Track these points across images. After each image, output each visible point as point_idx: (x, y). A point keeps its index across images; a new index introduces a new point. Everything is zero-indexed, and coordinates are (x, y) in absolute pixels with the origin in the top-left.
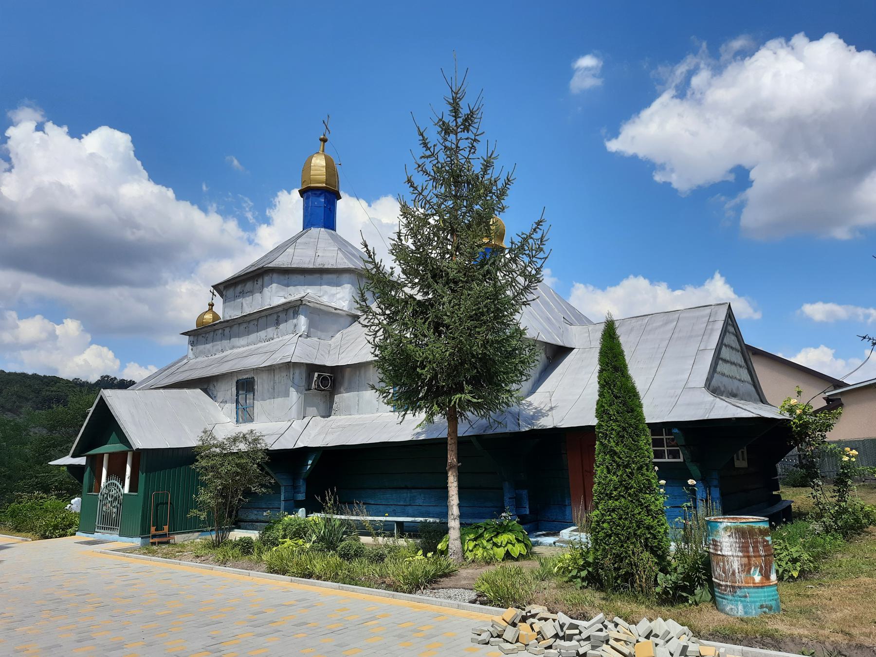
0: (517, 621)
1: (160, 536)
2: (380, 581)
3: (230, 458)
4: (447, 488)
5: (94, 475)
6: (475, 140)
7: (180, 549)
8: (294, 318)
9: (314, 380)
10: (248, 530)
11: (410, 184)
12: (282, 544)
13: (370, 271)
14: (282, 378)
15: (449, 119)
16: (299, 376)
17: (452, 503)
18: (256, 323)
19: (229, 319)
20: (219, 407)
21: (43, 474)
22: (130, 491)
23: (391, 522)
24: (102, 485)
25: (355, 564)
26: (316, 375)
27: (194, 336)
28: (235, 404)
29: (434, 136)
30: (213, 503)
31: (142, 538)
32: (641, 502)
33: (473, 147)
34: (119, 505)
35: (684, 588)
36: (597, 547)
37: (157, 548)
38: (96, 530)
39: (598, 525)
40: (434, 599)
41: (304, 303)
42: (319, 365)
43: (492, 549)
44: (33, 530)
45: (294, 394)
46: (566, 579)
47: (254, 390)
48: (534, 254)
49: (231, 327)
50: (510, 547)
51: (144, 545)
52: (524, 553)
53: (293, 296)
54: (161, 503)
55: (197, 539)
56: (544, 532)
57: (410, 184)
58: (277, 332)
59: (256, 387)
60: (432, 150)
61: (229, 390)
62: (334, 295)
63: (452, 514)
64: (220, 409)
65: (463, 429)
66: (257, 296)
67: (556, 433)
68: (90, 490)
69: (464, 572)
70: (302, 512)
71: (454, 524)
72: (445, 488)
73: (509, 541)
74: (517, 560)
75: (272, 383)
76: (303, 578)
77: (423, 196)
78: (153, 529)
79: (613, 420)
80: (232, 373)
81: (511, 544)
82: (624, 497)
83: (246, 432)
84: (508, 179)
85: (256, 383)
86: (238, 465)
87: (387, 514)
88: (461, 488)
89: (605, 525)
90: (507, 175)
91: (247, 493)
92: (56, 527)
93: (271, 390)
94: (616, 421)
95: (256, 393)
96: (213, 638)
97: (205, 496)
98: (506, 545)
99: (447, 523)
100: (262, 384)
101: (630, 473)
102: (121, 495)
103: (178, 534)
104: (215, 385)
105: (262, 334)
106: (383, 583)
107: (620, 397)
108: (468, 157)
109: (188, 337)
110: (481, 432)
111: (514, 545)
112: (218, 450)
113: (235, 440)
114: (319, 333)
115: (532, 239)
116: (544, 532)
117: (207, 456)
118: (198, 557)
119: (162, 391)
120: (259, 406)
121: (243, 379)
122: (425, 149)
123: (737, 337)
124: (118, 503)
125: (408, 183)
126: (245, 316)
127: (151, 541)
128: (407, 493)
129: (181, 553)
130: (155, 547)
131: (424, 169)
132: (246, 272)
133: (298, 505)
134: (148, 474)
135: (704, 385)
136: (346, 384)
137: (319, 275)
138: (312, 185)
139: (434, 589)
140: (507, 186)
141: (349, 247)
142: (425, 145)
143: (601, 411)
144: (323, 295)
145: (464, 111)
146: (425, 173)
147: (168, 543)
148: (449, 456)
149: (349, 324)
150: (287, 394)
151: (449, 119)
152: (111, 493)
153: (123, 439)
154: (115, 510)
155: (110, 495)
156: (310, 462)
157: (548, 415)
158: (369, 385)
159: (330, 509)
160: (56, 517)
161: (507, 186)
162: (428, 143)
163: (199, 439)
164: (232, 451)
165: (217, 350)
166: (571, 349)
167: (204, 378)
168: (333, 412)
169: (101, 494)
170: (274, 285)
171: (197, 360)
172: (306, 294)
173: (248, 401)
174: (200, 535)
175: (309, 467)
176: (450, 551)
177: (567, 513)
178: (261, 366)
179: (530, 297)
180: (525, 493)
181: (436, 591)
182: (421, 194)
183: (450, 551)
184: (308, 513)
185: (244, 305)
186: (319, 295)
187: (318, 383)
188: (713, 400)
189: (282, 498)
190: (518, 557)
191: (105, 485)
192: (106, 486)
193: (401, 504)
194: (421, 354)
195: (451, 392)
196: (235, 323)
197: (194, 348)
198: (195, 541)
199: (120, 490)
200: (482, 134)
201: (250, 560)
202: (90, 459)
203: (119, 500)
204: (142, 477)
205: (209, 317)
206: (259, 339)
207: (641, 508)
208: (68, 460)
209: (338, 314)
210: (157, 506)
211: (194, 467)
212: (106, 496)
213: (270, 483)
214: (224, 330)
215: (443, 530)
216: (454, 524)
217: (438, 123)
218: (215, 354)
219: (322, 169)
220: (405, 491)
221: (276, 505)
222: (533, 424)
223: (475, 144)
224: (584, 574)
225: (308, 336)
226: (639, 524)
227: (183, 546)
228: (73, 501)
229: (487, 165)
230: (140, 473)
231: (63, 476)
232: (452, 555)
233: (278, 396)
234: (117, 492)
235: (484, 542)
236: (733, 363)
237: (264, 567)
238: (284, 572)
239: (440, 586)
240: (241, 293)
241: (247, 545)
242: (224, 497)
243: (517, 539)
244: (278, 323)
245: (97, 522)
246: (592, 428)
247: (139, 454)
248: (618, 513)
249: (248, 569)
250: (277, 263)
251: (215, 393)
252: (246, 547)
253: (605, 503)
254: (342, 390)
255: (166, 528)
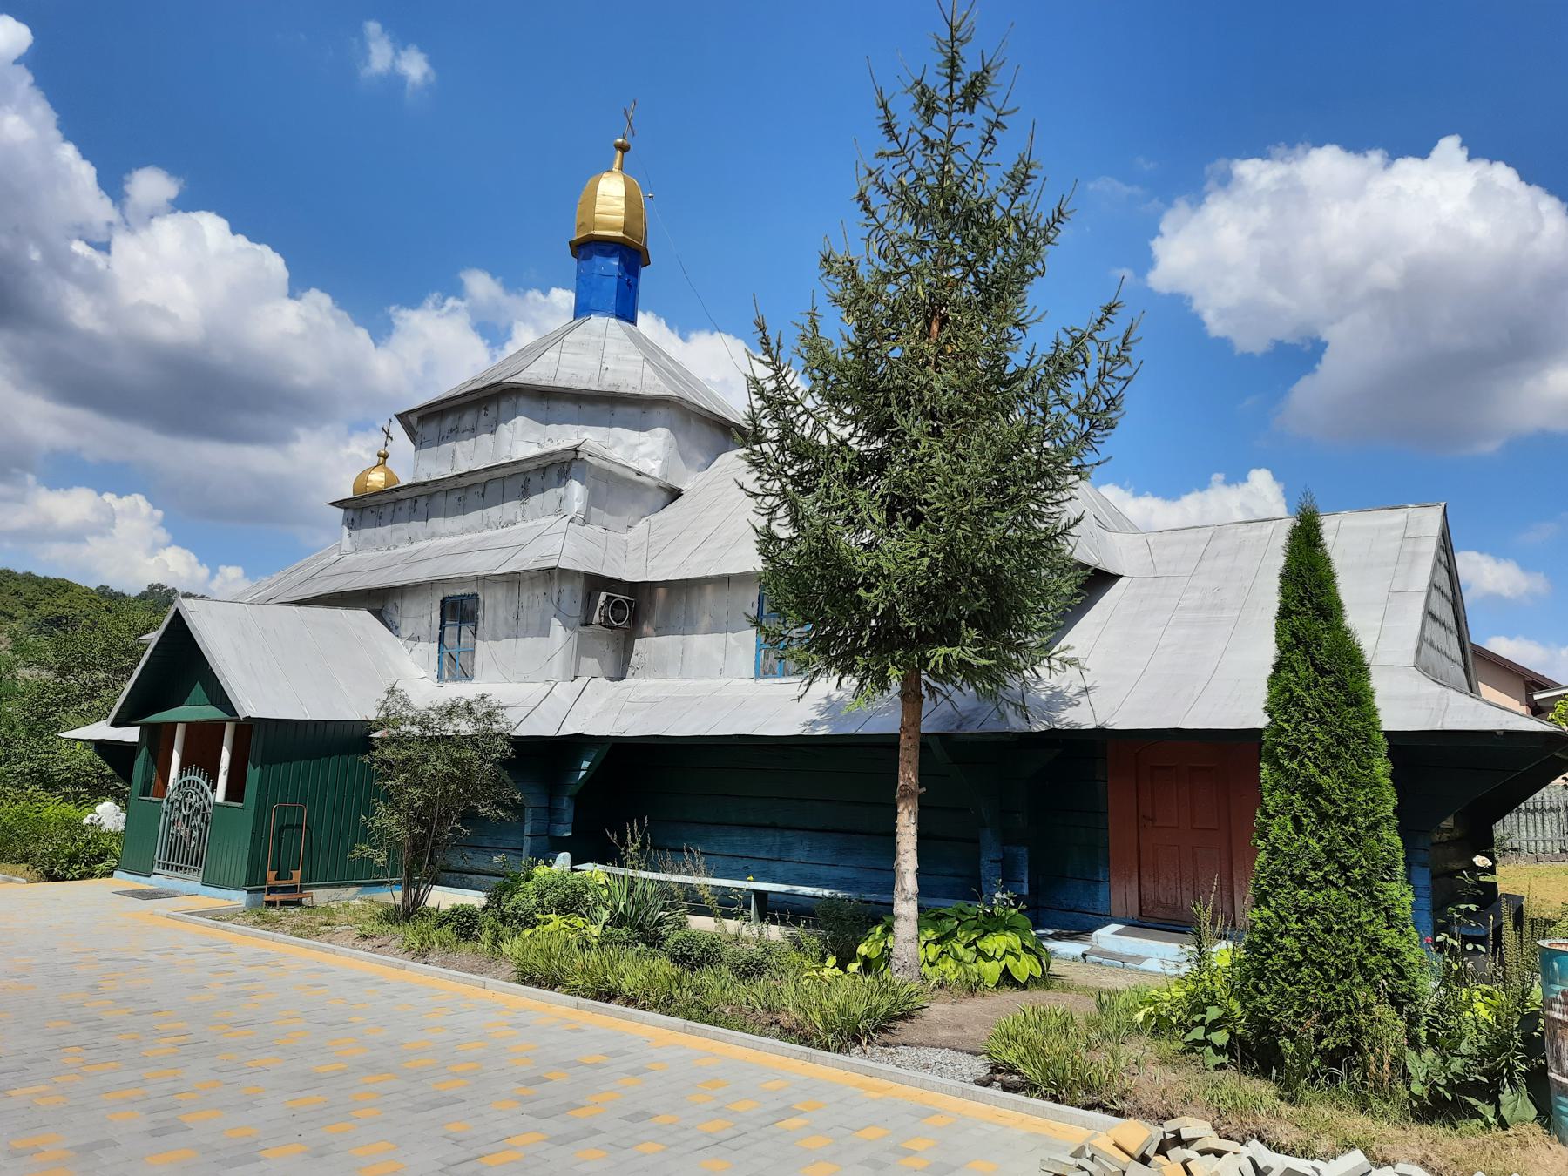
0: (1150, 1152)
1: (285, 890)
2: (767, 1019)
3: (442, 748)
4: (895, 835)
5: (155, 763)
6: (997, 124)
7: (325, 919)
8: (559, 485)
9: (599, 607)
10: (453, 886)
11: (862, 202)
12: (544, 924)
13: (761, 382)
14: (533, 599)
15: (936, 82)
16: (572, 596)
17: (903, 867)
18: (481, 491)
19: (425, 479)
20: (404, 648)
21: (43, 755)
22: (226, 799)
23: (780, 896)
24: (170, 784)
25: (706, 977)
26: (603, 596)
27: (355, 509)
28: (437, 644)
29: (906, 115)
30: (403, 833)
31: (249, 892)
32: (1376, 898)
33: (990, 139)
34: (203, 826)
35: (1478, 1090)
36: (1262, 986)
37: (279, 913)
38: (156, 870)
39: (1269, 939)
40: (892, 1068)
41: (581, 456)
42: (609, 579)
43: (975, 962)
44: (26, 861)
45: (557, 628)
46: (1180, 1046)
47: (477, 618)
48: (1107, 370)
49: (430, 496)
50: (1010, 960)
51: (252, 906)
52: (1038, 973)
53: (556, 443)
54: (288, 826)
55: (348, 899)
56: (1050, 932)
57: (862, 202)
58: (524, 511)
59: (480, 613)
60: (902, 140)
61: (424, 616)
62: (635, 447)
63: (903, 890)
64: (406, 651)
65: (932, 719)
66: (485, 438)
67: (1101, 740)
68: (145, 792)
69: (938, 1010)
70: (564, 858)
71: (906, 909)
72: (890, 836)
73: (1010, 950)
74: (1024, 987)
75: (514, 607)
76: (595, 999)
77: (885, 231)
78: (271, 875)
79: (1312, 719)
80: (432, 583)
81: (1013, 954)
82: (1336, 886)
83: (473, 698)
84: (1059, 210)
85: (481, 605)
86: (455, 762)
87: (751, 878)
88: (923, 838)
89: (1286, 941)
90: (1058, 203)
91: (470, 817)
92: (73, 859)
93: (510, 619)
94: (1322, 722)
95: (480, 625)
96: (457, 1142)
97: (387, 819)
98: (1003, 957)
99: (892, 905)
100: (493, 608)
101: (1352, 834)
102: (210, 805)
103: (318, 887)
104: (399, 604)
105: (493, 512)
106: (772, 1023)
107: (1332, 672)
108: (977, 161)
109: (343, 510)
110: (952, 728)
111: (1018, 957)
112: (416, 730)
113: (451, 711)
114: (607, 518)
115: (1093, 341)
116: (1050, 932)
117: (395, 741)
118: (365, 937)
119: (294, 608)
120: (485, 650)
121: (454, 596)
122: (888, 138)
123: (1448, 572)
124: (203, 821)
125: (860, 200)
126: (460, 476)
127: (268, 898)
128: (774, 836)
129: (329, 928)
130: (274, 912)
131: (880, 181)
132: (464, 391)
133: (558, 845)
134: (266, 766)
135: (1412, 662)
136: (657, 616)
137: (607, 407)
138: (597, 232)
139: (887, 1045)
140: (1056, 225)
141: (662, 358)
142: (889, 128)
143: (1282, 698)
144: (613, 446)
145: (969, 68)
146: (882, 190)
147: (298, 903)
148: (901, 772)
149: (660, 507)
150: (544, 631)
151: (936, 82)
152: (188, 800)
153: (219, 697)
154: (195, 834)
155: (185, 804)
156: (585, 765)
157: (1079, 703)
158: (748, 616)
159: (632, 859)
160: (75, 839)
161: (1056, 225)
162: (896, 126)
163: (379, 704)
164: (444, 733)
165: (400, 540)
166: (1122, 576)
167: (379, 589)
168: (630, 671)
169: (168, 800)
170: (520, 420)
171: (359, 555)
172: (581, 441)
173: (462, 640)
174: (360, 892)
175: (583, 773)
176: (897, 962)
177: (1102, 895)
178: (495, 573)
179: (1089, 458)
180: (1023, 853)
181: (892, 1050)
182: (881, 226)
183: (897, 962)
184: (575, 860)
185: (458, 453)
186: (605, 444)
187: (606, 612)
188: (1441, 693)
189: (527, 830)
190: (1027, 982)
191: (177, 784)
192: (179, 786)
193: (762, 856)
194: (865, 560)
195: (926, 640)
196: (439, 488)
197: (355, 533)
198: (352, 902)
199: (206, 797)
200: (1015, 111)
201: (475, 952)
202: (151, 732)
203: (203, 815)
204: (253, 774)
205: (377, 479)
206: (485, 522)
207: (1375, 912)
208: (102, 730)
209: (642, 484)
210: (281, 829)
211: (368, 761)
212: (177, 804)
213: (513, 800)
214: (416, 501)
215: (880, 915)
216: (906, 909)
217: (912, 88)
218: (396, 547)
219: (617, 202)
220: (770, 832)
221: (513, 844)
222: (1050, 719)
223: (996, 133)
224: (1221, 1038)
225: (585, 522)
226: (1373, 944)
227: (329, 912)
228: (99, 808)
229: (1020, 180)
230: (250, 767)
231: (81, 761)
232: (901, 972)
233: (526, 634)
234: (201, 800)
235: (960, 948)
236: (1443, 624)
237: (509, 968)
238: (552, 983)
239: (899, 1040)
240: (451, 431)
241: (467, 921)
242: (424, 824)
243: (1024, 947)
244: (525, 494)
245: (157, 853)
246: (1256, 733)
247: (249, 729)
248: (1322, 917)
249: (475, 970)
250: (528, 377)
251: (397, 620)
252: (464, 925)
253: (1289, 893)
254: (646, 628)
255: (297, 875)
